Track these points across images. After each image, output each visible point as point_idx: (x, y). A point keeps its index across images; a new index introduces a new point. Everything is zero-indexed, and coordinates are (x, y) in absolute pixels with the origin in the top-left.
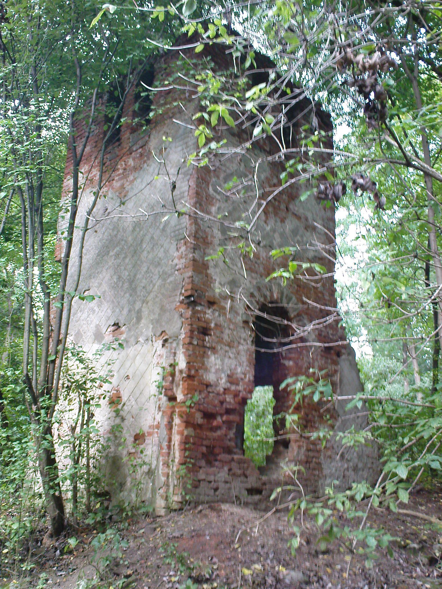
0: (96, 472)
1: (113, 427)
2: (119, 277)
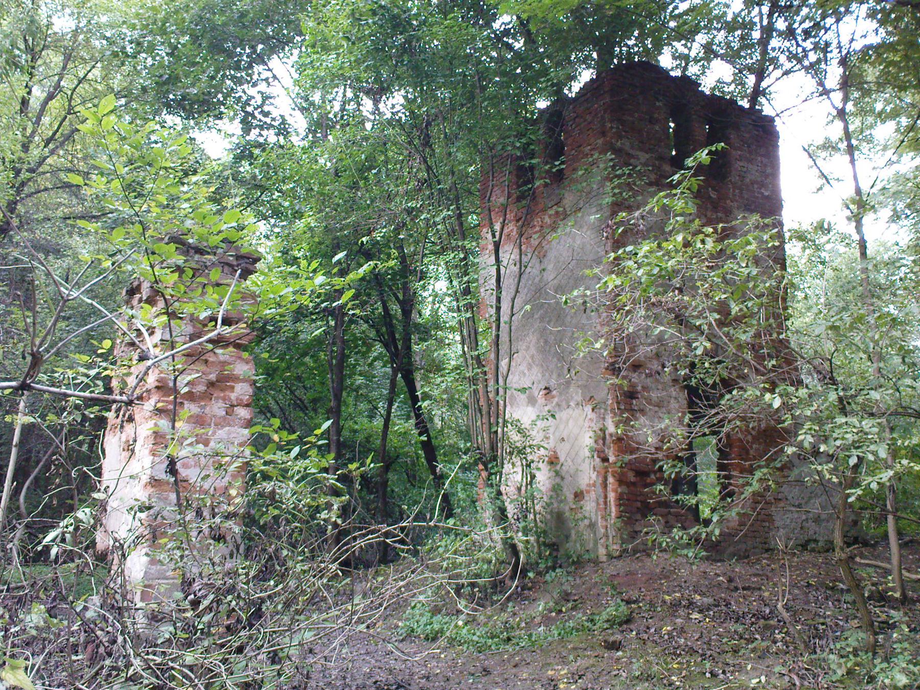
0: (543, 526)
1: (554, 486)
2: (546, 342)
